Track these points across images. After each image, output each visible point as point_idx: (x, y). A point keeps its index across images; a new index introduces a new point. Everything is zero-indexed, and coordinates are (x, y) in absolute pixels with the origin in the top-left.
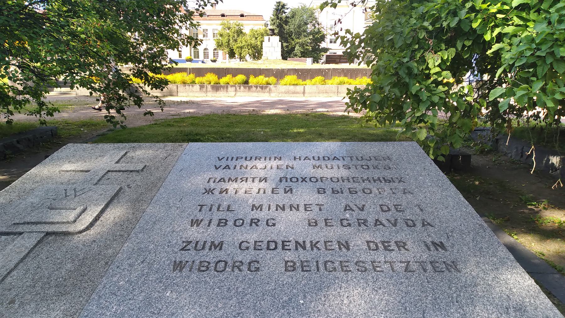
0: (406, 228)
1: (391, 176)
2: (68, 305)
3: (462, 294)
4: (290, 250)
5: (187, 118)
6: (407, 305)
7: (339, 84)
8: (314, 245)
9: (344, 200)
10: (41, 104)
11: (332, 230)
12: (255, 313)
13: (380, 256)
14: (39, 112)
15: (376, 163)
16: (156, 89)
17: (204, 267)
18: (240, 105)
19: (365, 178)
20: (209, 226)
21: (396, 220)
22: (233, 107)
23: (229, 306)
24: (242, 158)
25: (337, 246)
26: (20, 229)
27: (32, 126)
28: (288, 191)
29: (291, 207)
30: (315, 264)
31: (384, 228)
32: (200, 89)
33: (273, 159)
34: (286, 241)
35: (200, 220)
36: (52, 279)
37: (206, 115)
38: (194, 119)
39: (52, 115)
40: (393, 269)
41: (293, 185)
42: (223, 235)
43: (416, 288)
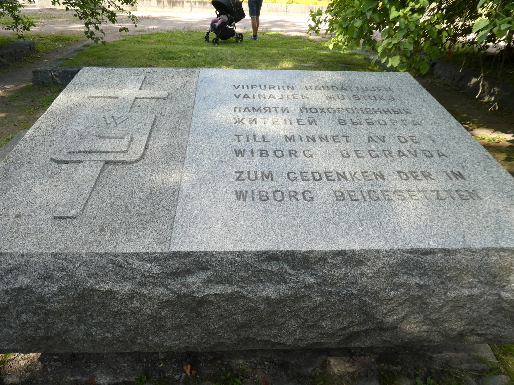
0: (426, 159)
1: (398, 108)
2: (155, 233)
3: (489, 220)
4: (334, 180)
5: (152, 34)
6: (448, 230)
7: (288, 3)
8: (353, 176)
9: (365, 132)
10: (17, 19)
11: (365, 161)
12: (324, 239)
13: (412, 184)
14: (16, 27)
15: (380, 94)
16: (127, 4)
17: (264, 197)
18: (199, 22)
19: (376, 109)
20: (253, 156)
21: (415, 151)
22: (192, 24)
23: (300, 233)
24: (257, 86)
25: (374, 177)
26: (77, 158)
27: (9, 39)
28: (312, 122)
29: (320, 138)
30: (360, 193)
31: (408, 159)
32: (158, 4)
33: (286, 88)
34: (327, 172)
35: (242, 150)
36: (129, 207)
37: (170, 32)
38: (161, 36)
39: (28, 29)
40: (426, 197)
41: (315, 116)
42: (269, 165)
43: (451, 215)
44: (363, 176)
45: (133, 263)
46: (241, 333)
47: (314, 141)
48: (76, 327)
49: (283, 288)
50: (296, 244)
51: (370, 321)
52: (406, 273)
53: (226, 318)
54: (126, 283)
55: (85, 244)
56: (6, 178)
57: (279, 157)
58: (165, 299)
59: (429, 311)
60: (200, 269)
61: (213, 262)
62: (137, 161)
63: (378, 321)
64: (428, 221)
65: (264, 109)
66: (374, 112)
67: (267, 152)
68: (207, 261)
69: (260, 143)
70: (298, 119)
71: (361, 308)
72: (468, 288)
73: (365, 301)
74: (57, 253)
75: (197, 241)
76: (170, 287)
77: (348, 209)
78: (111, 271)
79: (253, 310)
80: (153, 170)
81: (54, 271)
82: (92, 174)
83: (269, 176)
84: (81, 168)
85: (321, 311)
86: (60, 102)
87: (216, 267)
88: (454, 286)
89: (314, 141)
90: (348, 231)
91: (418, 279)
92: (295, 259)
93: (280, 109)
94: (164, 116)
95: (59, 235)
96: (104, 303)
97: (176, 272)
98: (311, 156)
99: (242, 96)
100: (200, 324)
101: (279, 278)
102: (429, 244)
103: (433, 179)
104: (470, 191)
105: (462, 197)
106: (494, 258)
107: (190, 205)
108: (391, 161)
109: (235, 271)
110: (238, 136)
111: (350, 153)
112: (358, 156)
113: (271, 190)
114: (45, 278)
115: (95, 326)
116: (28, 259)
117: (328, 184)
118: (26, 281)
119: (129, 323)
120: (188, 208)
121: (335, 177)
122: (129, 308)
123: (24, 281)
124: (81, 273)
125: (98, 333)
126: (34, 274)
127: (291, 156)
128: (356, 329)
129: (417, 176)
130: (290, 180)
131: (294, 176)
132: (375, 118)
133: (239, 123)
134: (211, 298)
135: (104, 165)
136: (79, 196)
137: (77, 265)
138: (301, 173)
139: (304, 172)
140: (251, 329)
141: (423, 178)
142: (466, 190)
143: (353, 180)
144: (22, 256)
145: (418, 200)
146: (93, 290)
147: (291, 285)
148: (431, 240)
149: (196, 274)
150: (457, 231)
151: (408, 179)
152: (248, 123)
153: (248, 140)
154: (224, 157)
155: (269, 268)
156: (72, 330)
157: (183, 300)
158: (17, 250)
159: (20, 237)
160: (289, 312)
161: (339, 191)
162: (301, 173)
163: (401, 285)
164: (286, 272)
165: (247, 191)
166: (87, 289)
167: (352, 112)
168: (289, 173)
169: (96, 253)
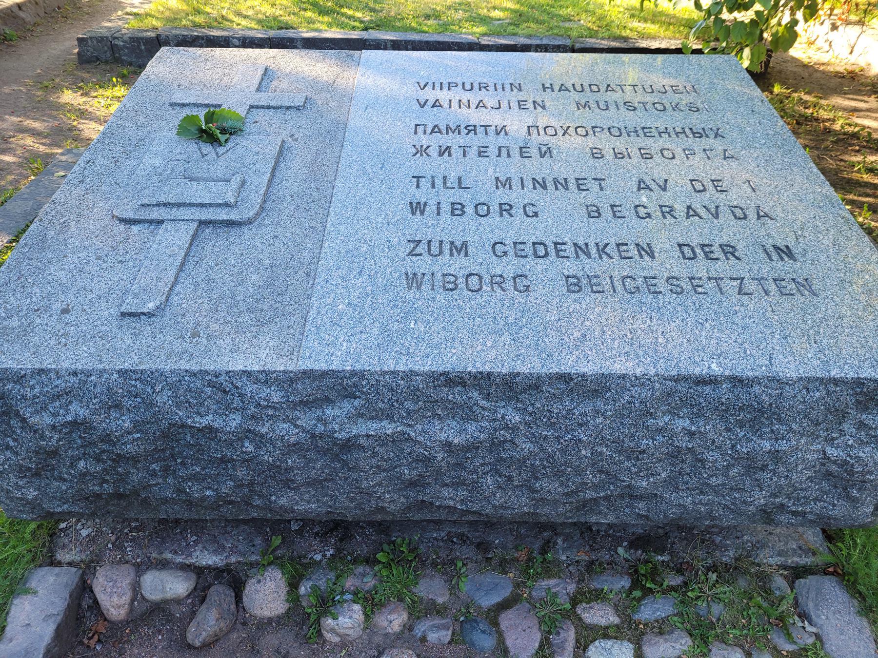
0: (733, 222)
1: (702, 126)
3: (821, 330)
4: (568, 257)
9: (634, 172)
11: (625, 225)
17: (450, 284)
19: (662, 128)
25: (636, 252)
26: (155, 214)
28: (545, 153)
30: (608, 280)
31: (701, 222)
34: (559, 244)
35: (422, 203)
36: (238, 298)
40: (720, 289)
43: (756, 321)
44: (619, 250)
45: (242, 386)
46: (411, 494)
47: (544, 187)
48: (160, 480)
49: (472, 427)
50: (494, 361)
51: (612, 483)
52: (669, 412)
53: (384, 470)
54: (232, 416)
55: (169, 356)
56: (43, 249)
57: (482, 216)
58: (292, 440)
59: (706, 473)
60: (346, 397)
61: (363, 387)
62: (250, 222)
63: (624, 484)
64: (716, 330)
65: (466, 128)
66: (657, 135)
67: (463, 206)
68: (355, 385)
69: (453, 191)
70: (521, 148)
71: (595, 464)
72: (770, 439)
73: (601, 453)
74: (126, 371)
75: (339, 354)
76: (299, 423)
77: (584, 307)
78: (210, 397)
79: (427, 461)
80: (277, 237)
81: (123, 396)
82: (178, 242)
83: (462, 249)
84: (161, 232)
85: (532, 465)
86: (124, 114)
87: (369, 394)
88: (748, 436)
89: (544, 187)
90: (578, 344)
91: (688, 422)
92: (491, 385)
93: (493, 128)
94: (296, 140)
95: (130, 342)
96: (201, 445)
97: (307, 400)
98: (536, 215)
99: (430, 103)
100: (346, 479)
101: (467, 413)
102: (709, 368)
103: (738, 259)
104: (800, 280)
105: (783, 290)
106: (818, 394)
107: (332, 295)
108: (670, 225)
109: (397, 401)
110: (418, 177)
111: (601, 210)
112: (615, 216)
113: (462, 272)
114: (110, 408)
115: (189, 479)
116: (83, 378)
117: (558, 263)
118: (83, 412)
119: (240, 475)
120: (330, 301)
121: (570, 250)
122: (238, 453)
123: (78, 411)
124: (163, 399)
125: (195, 490)
126: (94, 401)
127: (501, 215)
128: (590, 494)
129: (712, 252)
130: (496, 256)
131: (503, 248)
132: (654, 145)
133: (421, 155)
134: (362, 441)
135: (198, 226)
136: (159, 279)
137: (158, 388)
138: (515, 243)
139: (521, 243)
140: (425, 488)
141: (722, 256)
142: (793, 280)
143: (601, 257)
144: (75, 374)
145: (705, 293)
146: (184, 426)
147: (485, 424)
148: (714, 361)
149: (338, 404)
150: (761, 348)
151: (695, 257)
152: (436, 154)
153: (433, 186)
154: (391, 215)
155: (451, 398)
156: (155, 485)
157: (320, 443)
158: (66, 365)
159: (70, 345)
160: (482, 465)
161: (574, 277)
162: (515, 243)
163: (659, 431)
164: (477, 404)
165: (424, 274)
166: (174, 425)
167: (612, 130)
168: (496, 243)
169: (187, 371)
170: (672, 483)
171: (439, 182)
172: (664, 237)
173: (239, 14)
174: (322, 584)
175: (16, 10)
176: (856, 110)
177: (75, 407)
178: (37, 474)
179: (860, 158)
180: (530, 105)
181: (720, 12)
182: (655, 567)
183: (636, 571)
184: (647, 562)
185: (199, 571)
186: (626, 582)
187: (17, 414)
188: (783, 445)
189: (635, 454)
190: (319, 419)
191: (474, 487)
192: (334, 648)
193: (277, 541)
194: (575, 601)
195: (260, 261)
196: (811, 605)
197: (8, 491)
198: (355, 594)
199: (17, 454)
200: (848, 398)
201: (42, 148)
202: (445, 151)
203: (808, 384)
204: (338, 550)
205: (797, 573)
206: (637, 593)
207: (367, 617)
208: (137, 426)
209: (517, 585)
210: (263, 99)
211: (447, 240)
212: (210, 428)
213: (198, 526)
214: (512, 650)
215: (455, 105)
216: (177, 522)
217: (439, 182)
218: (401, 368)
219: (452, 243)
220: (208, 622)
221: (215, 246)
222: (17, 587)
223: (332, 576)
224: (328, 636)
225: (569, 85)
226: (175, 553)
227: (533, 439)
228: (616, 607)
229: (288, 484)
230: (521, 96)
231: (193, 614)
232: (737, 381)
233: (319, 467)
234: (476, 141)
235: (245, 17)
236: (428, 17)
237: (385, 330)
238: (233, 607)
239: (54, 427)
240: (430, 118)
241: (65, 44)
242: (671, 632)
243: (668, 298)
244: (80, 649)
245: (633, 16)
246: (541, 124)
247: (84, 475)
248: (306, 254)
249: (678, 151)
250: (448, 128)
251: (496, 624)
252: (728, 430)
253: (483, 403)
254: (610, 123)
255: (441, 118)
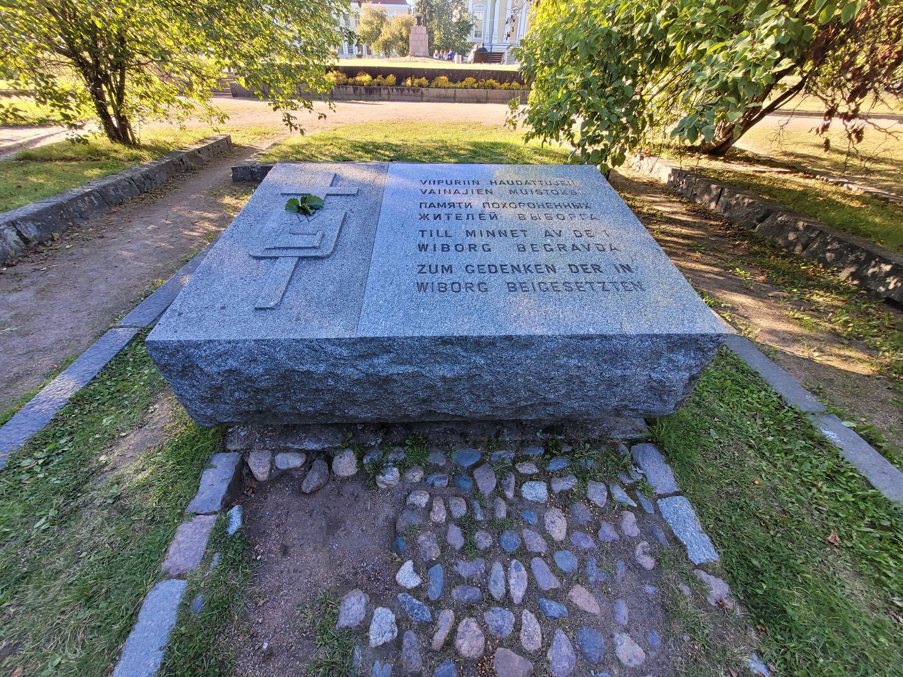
17: (442, 288)
19: (557, 204)
47: (494, 235)
49: (457, 368)
52: (566, 356)
55: (283, 331)
62: (328, 257)
68: (390, 345)
73: (529, 380)
79: (432, 387)
83: (449, 269)
89: (494, 235)
95: (260, 324)
98: (489, 250)
99: (428, 191)
101: (454, 360)
110: (423, 231)
121: (509, 269)
123: (232, 363)
124: (281, 355)
128: (523, 403)
132: (553, 212)
134: (395, 377)
144: (229, 342)
146: (294, 371)
158: (224, 337)
163: (561, 366)
170: (567, 396)
171: (434, 234)
172: (561, 262)
173: (321, 153)
174: (376, 457)
175: (197, 152)
176: (654, 202)
177: (230, 361)
178: (211, 401)
179: (657, 227)
180: (484, 192)
181: (585, 145)
182: (557, 442)
183: (547, 445)
184: (552, 440)
185: (307, 453)
186: (542, 451)
187: (197, 366)
188: (628, 372)
189: (548, 380)
190: (370, 365)
191: (459, 401)
192: (384, 492)
193: (350, 435)
194: (514, 462)
195: (334, 278)
196: (640, 458)
197: (196, 411)
198: (394, 462)
199: (199, 389)
200: (663, 345)
201: (214, 228)
202: (437, 217)
203: (642, 337)
204: (384, 439)
205: (632, 443)
206: (548, 456)
207: (401, 474)
208: (266, 371)
209: (483, 455)
210: (334, 190)
211: (440, 264)
212: (308, 372)
213: (306, 428)
214: (481, 489)
215: (442, 192)
216: (294, 426)
217: (434, 234)
218: (416, 335)
219: (443, 266)
220: (313, 479)
221: (307, 270)
222: (205, 464)
223: (381, 453)
224: (380, 485)
225: (505, 181)
226: (294, 443)
227: (492, 373)
228: (536, 464)
229: (354, 402)
230: (479, 187)
231: (305, 476)
232: (603, 337)
233: (371, 392)
234: (454, 211)
235: (325, 155)
236: (425, 154)
237: (406, 314)
238: (327, 471)
239: (219, 373)
240: (428, 199)
241: (225, 171)
242: (566, 476)
243: (564, 294)
244: (243, 496)
245: (535, 153)
246: (490, 202)
247: (239, 400)
248: (360, 274)
249: (566, 215)
250: (438, 204)
251: (472, 476)
252: (599, 365)
253: (463, 354)
254: (528, 201)
255: (435, 199)
